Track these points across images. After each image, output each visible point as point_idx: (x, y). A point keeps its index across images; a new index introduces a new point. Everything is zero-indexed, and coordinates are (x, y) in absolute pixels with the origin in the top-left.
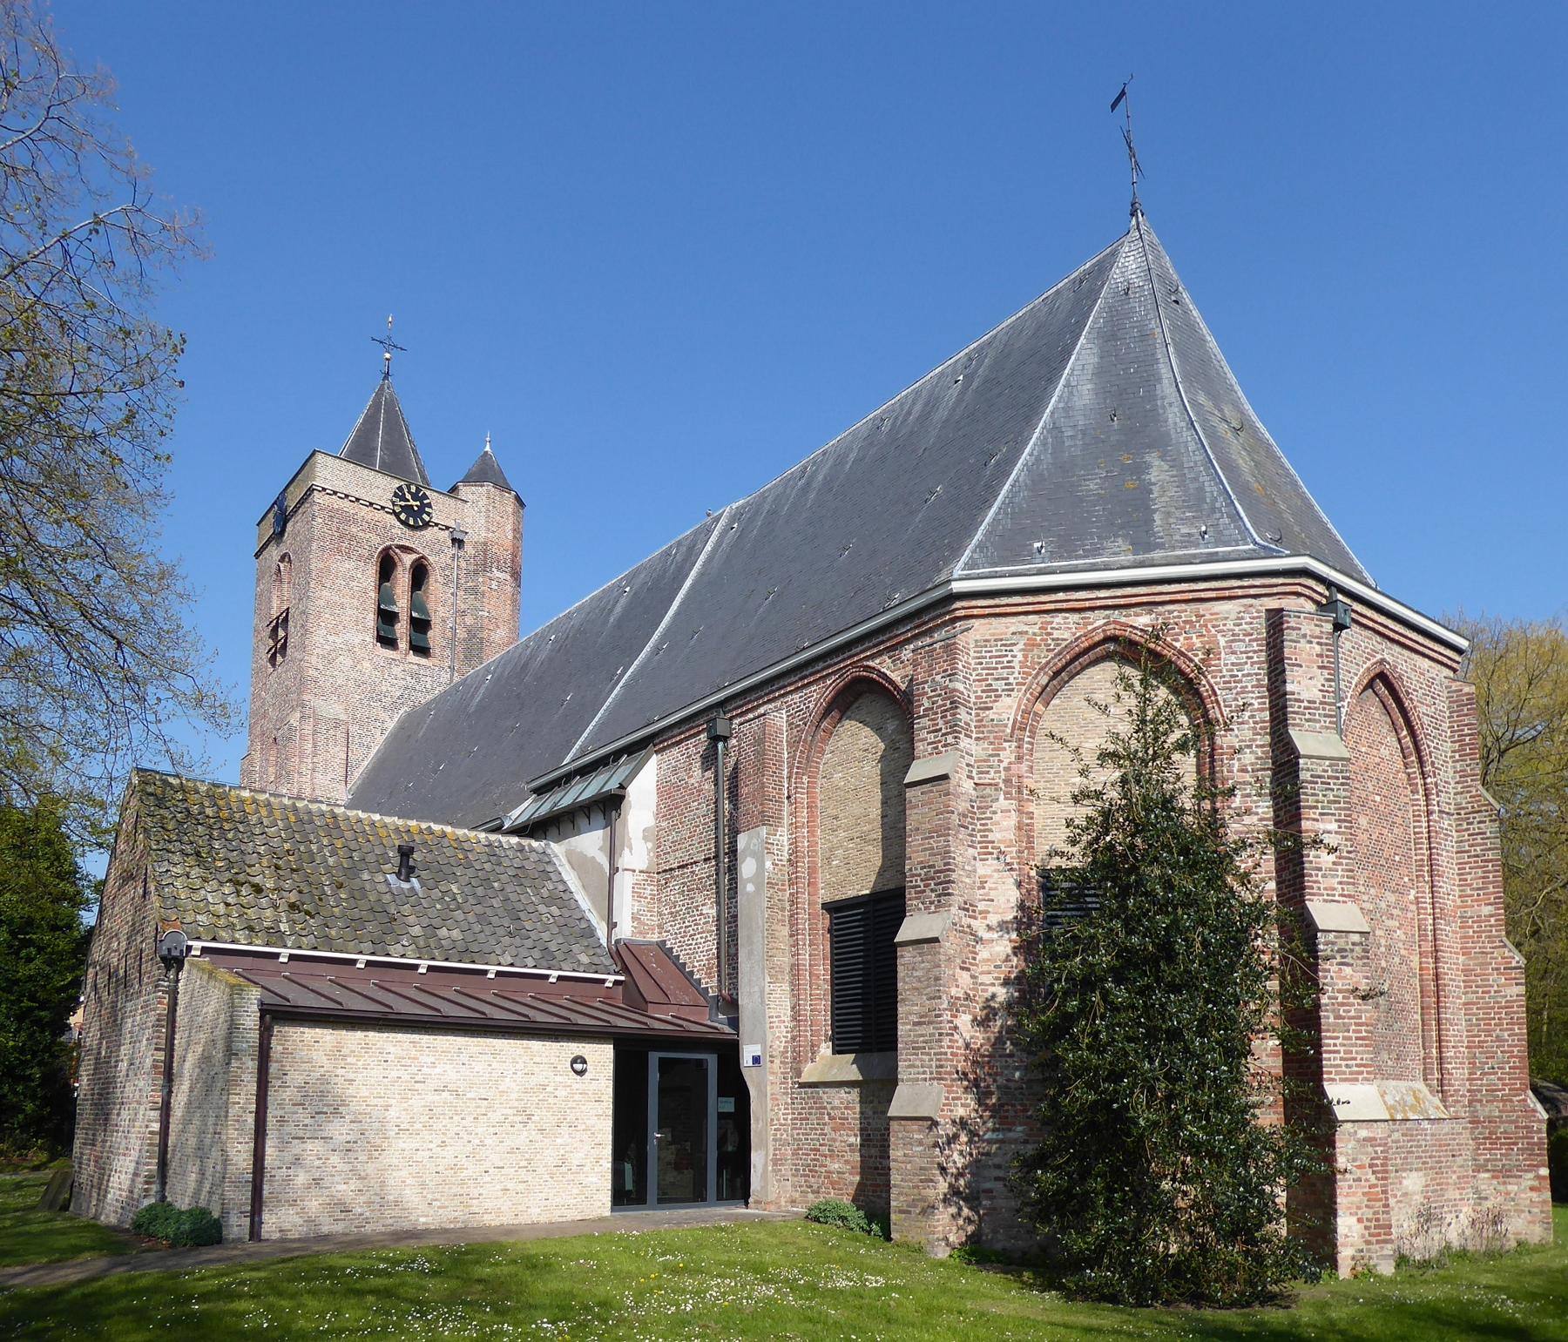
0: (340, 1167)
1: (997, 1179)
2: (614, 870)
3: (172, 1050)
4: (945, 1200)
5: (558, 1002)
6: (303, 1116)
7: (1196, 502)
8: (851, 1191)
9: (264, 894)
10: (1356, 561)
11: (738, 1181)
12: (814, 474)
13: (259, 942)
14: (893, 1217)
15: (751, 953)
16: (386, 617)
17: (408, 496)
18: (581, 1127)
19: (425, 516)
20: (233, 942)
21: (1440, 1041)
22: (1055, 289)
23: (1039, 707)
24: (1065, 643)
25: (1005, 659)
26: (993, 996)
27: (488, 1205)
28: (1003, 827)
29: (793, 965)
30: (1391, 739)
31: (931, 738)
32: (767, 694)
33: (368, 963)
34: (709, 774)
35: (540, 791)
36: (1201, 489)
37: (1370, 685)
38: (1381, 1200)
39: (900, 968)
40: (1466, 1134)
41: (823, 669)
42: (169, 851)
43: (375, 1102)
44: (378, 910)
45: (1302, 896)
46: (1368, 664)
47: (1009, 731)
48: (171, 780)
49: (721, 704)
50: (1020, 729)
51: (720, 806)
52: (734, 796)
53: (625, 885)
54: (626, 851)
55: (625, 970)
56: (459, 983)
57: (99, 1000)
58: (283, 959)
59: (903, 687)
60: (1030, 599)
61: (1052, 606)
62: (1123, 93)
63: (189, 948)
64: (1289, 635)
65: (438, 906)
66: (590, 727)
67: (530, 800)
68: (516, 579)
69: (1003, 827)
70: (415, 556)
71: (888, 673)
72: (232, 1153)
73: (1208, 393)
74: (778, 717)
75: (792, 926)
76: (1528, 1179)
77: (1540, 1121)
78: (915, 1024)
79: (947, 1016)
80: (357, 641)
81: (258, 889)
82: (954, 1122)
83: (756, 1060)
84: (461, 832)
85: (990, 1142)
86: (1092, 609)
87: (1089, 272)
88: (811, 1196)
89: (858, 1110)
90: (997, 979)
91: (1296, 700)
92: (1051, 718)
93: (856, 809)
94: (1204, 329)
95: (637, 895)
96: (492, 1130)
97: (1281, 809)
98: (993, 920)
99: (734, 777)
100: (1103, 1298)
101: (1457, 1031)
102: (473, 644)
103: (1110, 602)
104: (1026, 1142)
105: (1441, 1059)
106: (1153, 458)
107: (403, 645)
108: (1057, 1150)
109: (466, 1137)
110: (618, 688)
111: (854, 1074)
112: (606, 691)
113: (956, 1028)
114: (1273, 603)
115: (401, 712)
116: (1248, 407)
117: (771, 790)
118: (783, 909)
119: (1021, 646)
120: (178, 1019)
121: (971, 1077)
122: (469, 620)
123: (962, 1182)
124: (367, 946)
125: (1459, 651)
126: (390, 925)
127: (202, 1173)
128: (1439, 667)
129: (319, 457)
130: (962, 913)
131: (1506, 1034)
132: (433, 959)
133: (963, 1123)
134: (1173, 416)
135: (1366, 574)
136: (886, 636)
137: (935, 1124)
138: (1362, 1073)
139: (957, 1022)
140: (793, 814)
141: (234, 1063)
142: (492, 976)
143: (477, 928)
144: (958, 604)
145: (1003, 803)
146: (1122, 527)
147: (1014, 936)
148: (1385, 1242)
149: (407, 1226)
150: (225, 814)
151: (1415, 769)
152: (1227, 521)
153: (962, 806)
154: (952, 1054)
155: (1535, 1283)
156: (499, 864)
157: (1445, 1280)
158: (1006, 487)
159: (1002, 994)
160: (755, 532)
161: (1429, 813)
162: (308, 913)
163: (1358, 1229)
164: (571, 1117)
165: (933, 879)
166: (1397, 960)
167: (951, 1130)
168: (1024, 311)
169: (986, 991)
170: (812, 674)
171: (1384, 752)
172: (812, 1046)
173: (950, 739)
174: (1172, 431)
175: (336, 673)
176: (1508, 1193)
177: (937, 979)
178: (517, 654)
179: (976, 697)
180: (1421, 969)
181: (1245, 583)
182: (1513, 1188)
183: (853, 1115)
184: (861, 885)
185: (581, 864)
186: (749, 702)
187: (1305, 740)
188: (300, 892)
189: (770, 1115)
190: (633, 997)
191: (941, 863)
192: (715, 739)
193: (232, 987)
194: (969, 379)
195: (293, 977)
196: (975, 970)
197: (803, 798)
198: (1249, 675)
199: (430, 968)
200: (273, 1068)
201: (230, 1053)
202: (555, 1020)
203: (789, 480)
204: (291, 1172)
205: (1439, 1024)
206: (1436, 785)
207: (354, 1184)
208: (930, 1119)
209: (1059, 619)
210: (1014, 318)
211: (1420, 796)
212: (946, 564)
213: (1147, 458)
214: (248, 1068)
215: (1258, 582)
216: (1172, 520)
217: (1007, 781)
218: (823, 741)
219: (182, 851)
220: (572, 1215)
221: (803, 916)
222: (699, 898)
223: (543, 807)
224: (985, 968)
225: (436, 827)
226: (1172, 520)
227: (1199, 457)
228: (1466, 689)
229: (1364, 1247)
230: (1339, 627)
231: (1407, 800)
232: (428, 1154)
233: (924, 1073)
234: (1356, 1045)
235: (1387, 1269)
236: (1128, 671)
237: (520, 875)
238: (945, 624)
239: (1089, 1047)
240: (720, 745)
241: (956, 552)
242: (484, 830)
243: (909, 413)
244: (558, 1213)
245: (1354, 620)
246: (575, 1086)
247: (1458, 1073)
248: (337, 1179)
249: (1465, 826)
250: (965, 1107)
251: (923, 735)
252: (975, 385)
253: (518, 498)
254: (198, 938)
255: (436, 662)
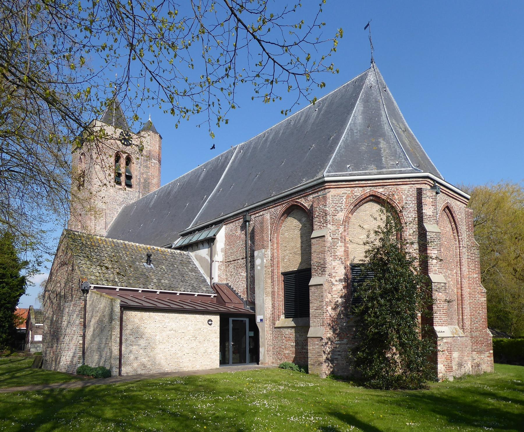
0: (143, 354)
1: (339, 355)
2: (212, 261)
3: (86, 318)
4: (325, 362)
5: (154, 299)
6: (132, 338)
7: (394, 155)
8: (292, 359)
9: (109, 269)
10: (438, 171)
11: (254, 357)
12: (268, 137)
13: (110, 285)
14: (309, 366)
15: (259, 287)
16: (119, 175)
17: (125, 135)
18: (211, 341)
19: (130, 141)
20: (103, 285)
21: (462, 314)
22: (347, 84)
23: (350, 215)
24: (358, 197)
25: (340, 201)
26: (338, 301)
27: (185, 365)
28: (340, 251)
29: (272, 291)
30: (449, 225)
31: (319, 224)
32: (263, 208)
33: (143, 291)
34: (243, 232)
35: (183, 235)
36: (396, 150)
37: (444, 210)
38: (449, 360)
39: (310, 293)
40: (469, 341)
41: (282, 202)
42: (79, 256)
43: (152, 334)
44: (143, 274)
45: (428, 272)
46: (444, 204)
47: (342, 222)
48: (76, 233)
49: (247, 211)
50: (345, 222)
51: (247, 242)
52: (252, 238)
53: (216, 266)
54: (216, 255)
55: (217, 292)
56: (168, 297)
57: (52, 302)
58: (158, 293)
59: (309, 208)
60: (348, 183)
61: (354, 185)
62: (368, 25)
63: (90, 287)
64: (424, 196)
65: (160, 273)
66: (198, 215)
67: (180, 238)
68: (160, 163)
69: (340, 251)
70: (126, 155)
71: (304, 204)
72: (113, 350)
73: (395, 120)
74: (267, 215)
75: (272, 279)
76: (487, 354)
77: (490, 337)
78: (315, 309)
79: (325, 307)
81: (107, 268)
82: (327, 338)
83: (261, 320)
84: (163, 249)
85: (336, 344)
86: (366, 186)
87: (358, 80)
88: (279, 361)
89: (294, 335)
90: (338, 296)
91: (426, 215)
92: (353, 218)
93: (292, 244)
94: (393, 100)
95: (220, 269)
96: (186, 342)
97: (421, 247)
98: (337, 278)
99: (253, 232)
100: (378, 388)
101: (467, 311)
102: (146, 185)
103: (371, 185)
104: (347, 344)
105: (463, 319)
106: (381, 140)
107: (123, 184)
108: (362, 346)
109: (179, 344)
110: (206, 203)
111: (293, 324)
112: (201, 203)
113: (327, 311)
114: (419, 186)
116: (406, 123)
117: (265, 238)
118: (269, 274)
119: (345, 197)
120: (87, 309)
121: (331, 325)
122: (145, 176)
123: (329, 356)
124: (141, 286)
125: (468, 199)
126: (147, 280)
127: (101, 356)
128: (462, 204)
130: (329, 276)
131: (481, 312)
132: (161, 289)
133: (329, 339)
134: (386, 127)
135: (441, 175)
136: (304, 192)
137: (322, 339)
138: (444, 323)
139: (328, 309)
140: (272, 245)
141: (113, 322)
142: (158, 293)
143: (172, 280)
144: (326, 184)
145: (340, 244)
146: (373, 161)
147: (344, 283)
148: (451, 371)
149: (162, 371)
150: (93, 244)
151: (456, 234)
152: (404, 160)
153: (328, 245)
154: (326, 318)
155: (493, 383)
156: (175, 259)
157: (468, 382)
158: (338, 147)
159: (340, 300)
160: (249, 154)
161: (460, 247)
162: (123, 275)
163: (443, 368)
164: (208, 338)
165: (320, 266)
166: (451, 290)
167: (326, 341)
168: (337, 89)
169: (335, 300)
170: (278, 203)
171: (448, 229)
172: (278, 316)
173: (325, 225)
174: (386, 132)
176: (481, 358)
177: (322, 296)
178: (165, 189)
179: (332, 212)
180: (457, 293)
181: (411, 180)
182: (482, 356)
183: (293, 337)
184: (294, 267)
185: (200, 259)
186: (257, 210)
187: (429, 227)
188: (119, 269)
189: (266, 337)
190: (220, 300)
191: (323, 262)
192: (245, 221)
193: (112, 299)
194: (320, 110)
195: (121, 295)
196: (332, 293)
197: (275, 240)
198: (412, 207)
199: (160, 292)
200: (124, 323)
201: (111, 319)
202: (202, 308)
203: (260, 137)
204: (129, 355)
205: (462, 309)
206: (462, 239)
207: (147, 359)
208: (321, 337)
209: (356, 189)
210: (333, 92)
211: (457, 242)
212: (320, 171)
213: (379, 140)
214: (116, 324)
215: (414, 180)
216: (388, 160)
217: (341, 237)
218: (282, 223)
219: (83, 256)
220: (209, 368)
221: (276, 276)
222: (240, 270)
223: (186, 241)
224: (335, 293)
225: (155, 247)
226: (388, 160)
227: (395, 140)
228: (470, 211)
229: (445, 373)
230: (437, 193)
231: (453, 243)
232: (168, 349)
233: (318, 324)
234: (442, 315)
235: (451, 379)
236: (383, 208)
237: (182, 263)
238: (322, 190)
239: (374, 316)
240: (247, 223)
241: (323, 167)
242: (165, 248)
243: (300, 119)
244: (204, 367)
245: (441, 191)
246: (209, 329)
247: (467, 323)
248: (142, 357)
249: (469, 251)
250: (330, 334)
251: (316, 223)
252: (322, 112)
253: (160, 136)
254: (93, 284)
255: (134, 190)
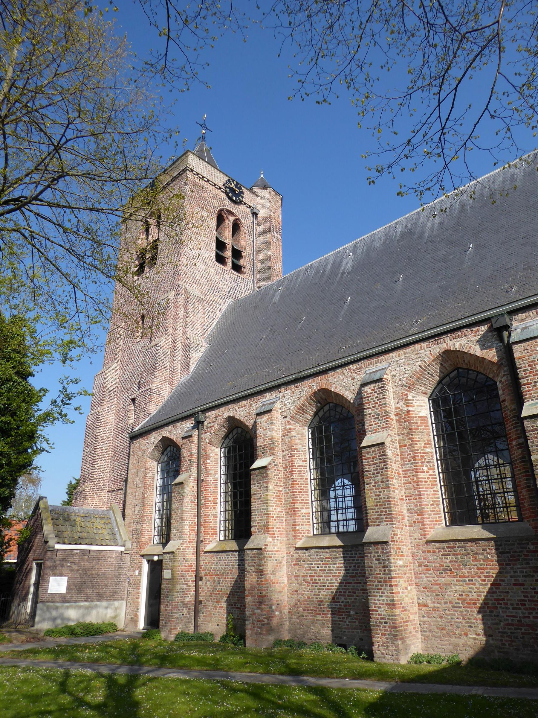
19: (240, 197)
70: (234, 218)
80: (207, 256)
115: (230, 301)
122: (262, 257)
129: (189, 153)
175: (196, 271)
